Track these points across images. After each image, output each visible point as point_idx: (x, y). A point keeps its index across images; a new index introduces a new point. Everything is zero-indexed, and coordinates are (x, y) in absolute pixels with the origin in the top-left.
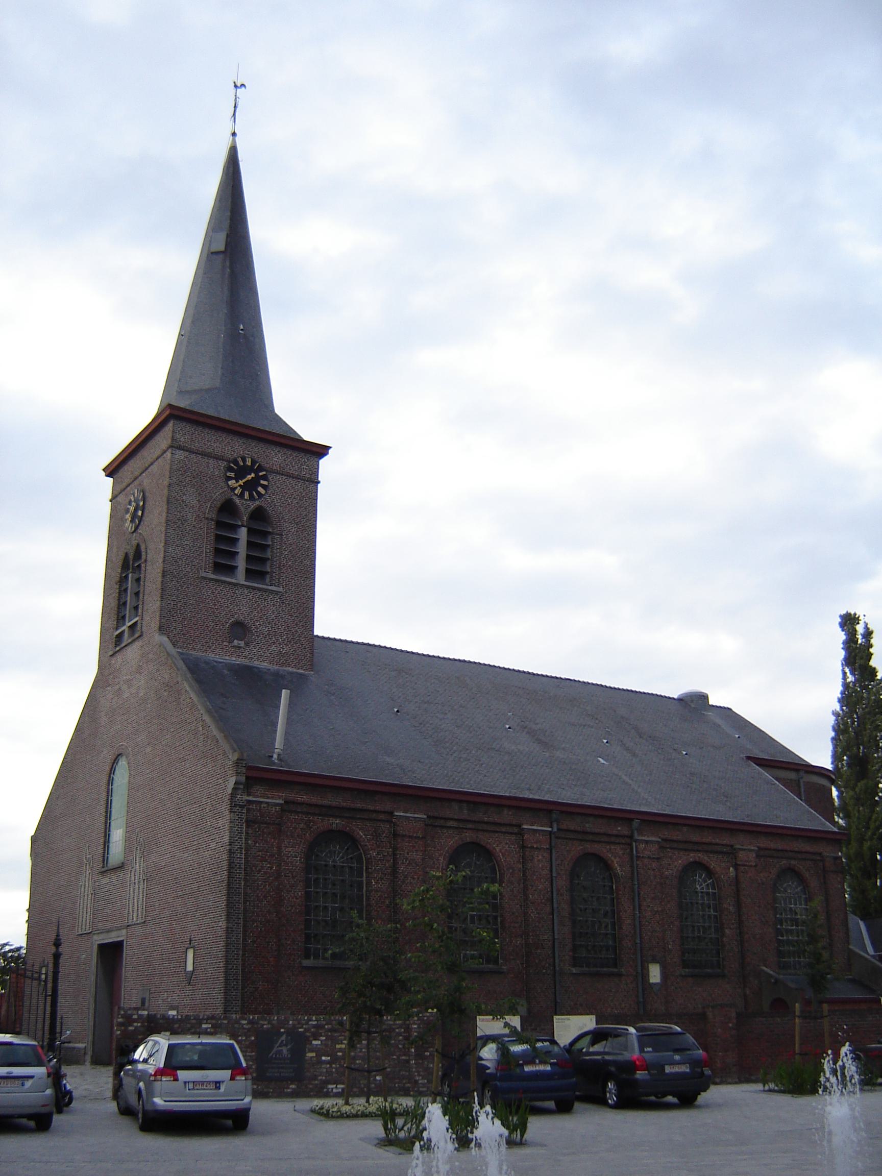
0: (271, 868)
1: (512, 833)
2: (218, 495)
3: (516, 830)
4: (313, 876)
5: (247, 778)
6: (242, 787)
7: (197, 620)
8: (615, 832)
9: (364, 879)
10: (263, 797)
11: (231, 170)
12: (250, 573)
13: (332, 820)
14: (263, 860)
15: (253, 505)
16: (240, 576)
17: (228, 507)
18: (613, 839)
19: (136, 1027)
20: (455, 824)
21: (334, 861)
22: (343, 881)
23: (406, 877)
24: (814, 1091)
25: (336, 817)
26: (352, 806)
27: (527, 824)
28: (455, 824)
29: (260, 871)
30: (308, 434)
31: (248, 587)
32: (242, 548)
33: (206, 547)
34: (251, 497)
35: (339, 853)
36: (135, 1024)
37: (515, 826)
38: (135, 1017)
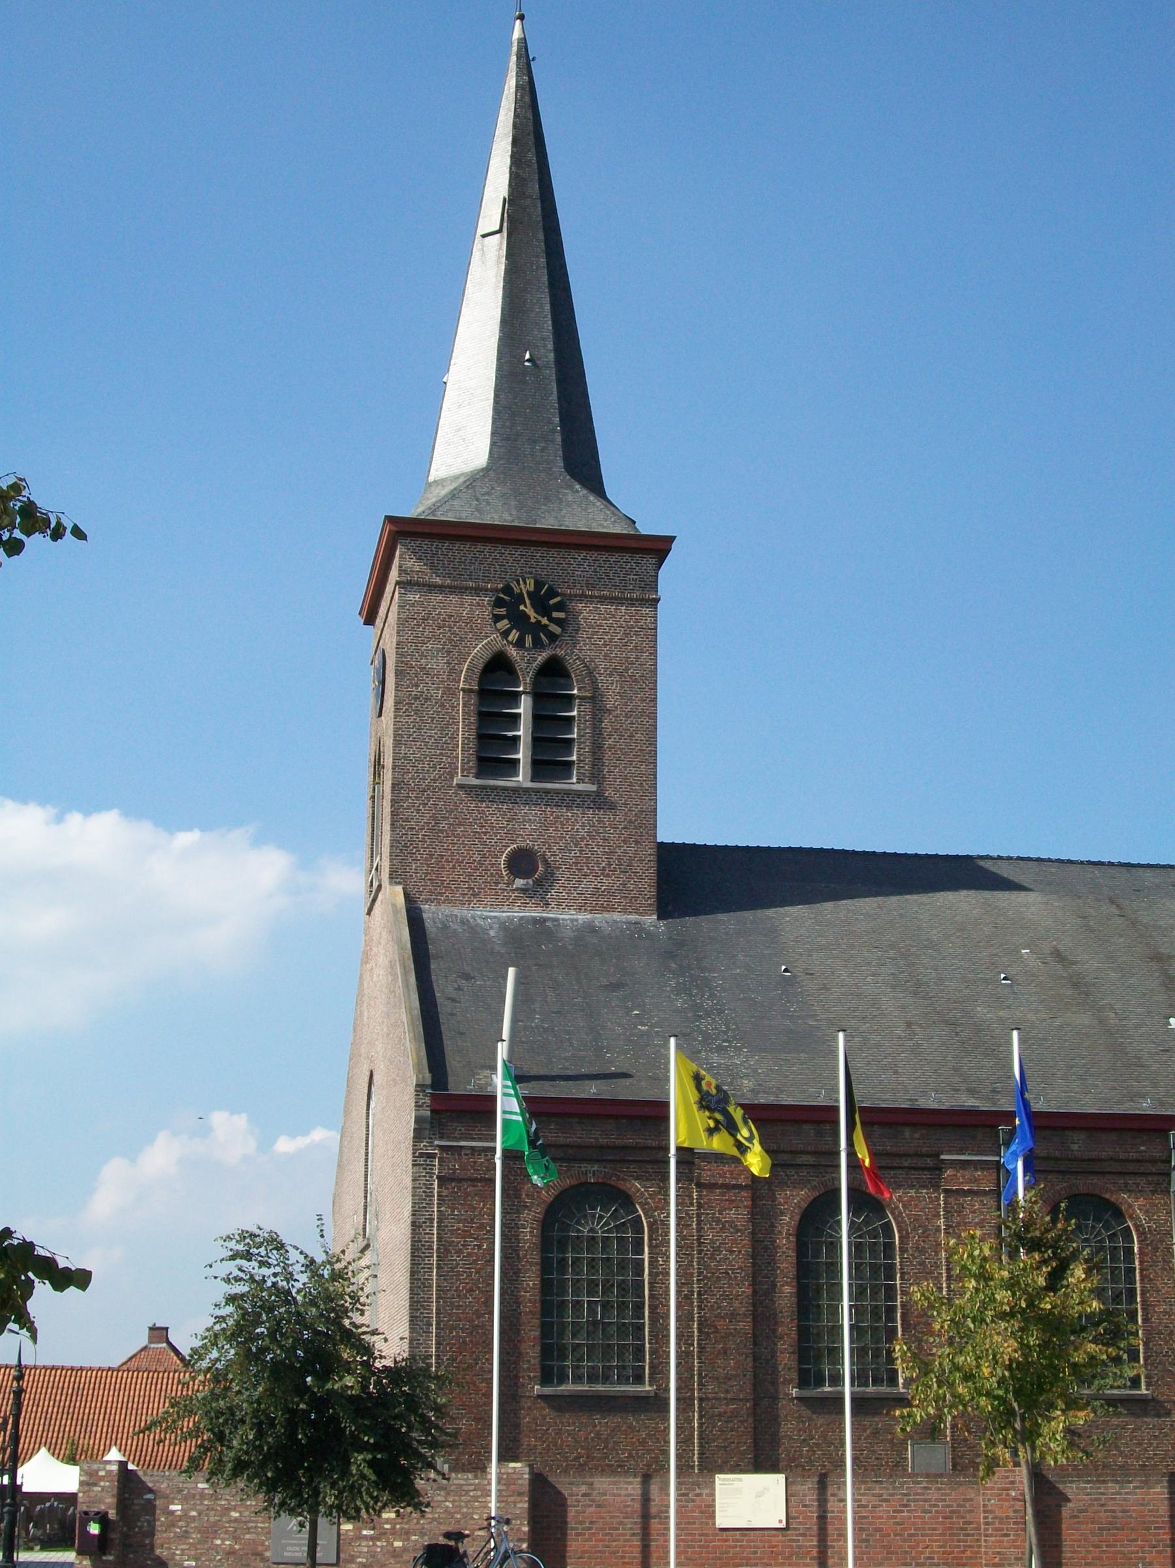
0: (480, 1247)
1: (923, 1169)
2: (479, 650)
3: (929, 1162)
4: (555, 1255)
5: (432, 1111)
6: (428, 1126)
7: (452, 854)
8: (1133, 1155)
9: (646, 1256)
10: (466, 1139)
11: (527, 99)
12: (540, 768)
13: (585, 1166)
14: (466, 1234)
15: (542, 657)
16: (522, 778)
17: (498, 666)
18: (1131, 1167)
19: (103, 1488)
20: (810, 1159)
21: (592, 1230)
22: (608, 1259)
23: (718, 1250)
24: (429, 1546)
25: (591, 1161)
26: (619, 1142)
27: (950, 1153)
28: (810, 1159)
29: (459, 1252)
30: (646, 528)
31: (536, 791)
32: (523, 732)
33: (463, 732)
34: (538, 644)
35: (601, 1217)
36: (102, 1484)
37: (930, 1156)
38: (102, 1473)
